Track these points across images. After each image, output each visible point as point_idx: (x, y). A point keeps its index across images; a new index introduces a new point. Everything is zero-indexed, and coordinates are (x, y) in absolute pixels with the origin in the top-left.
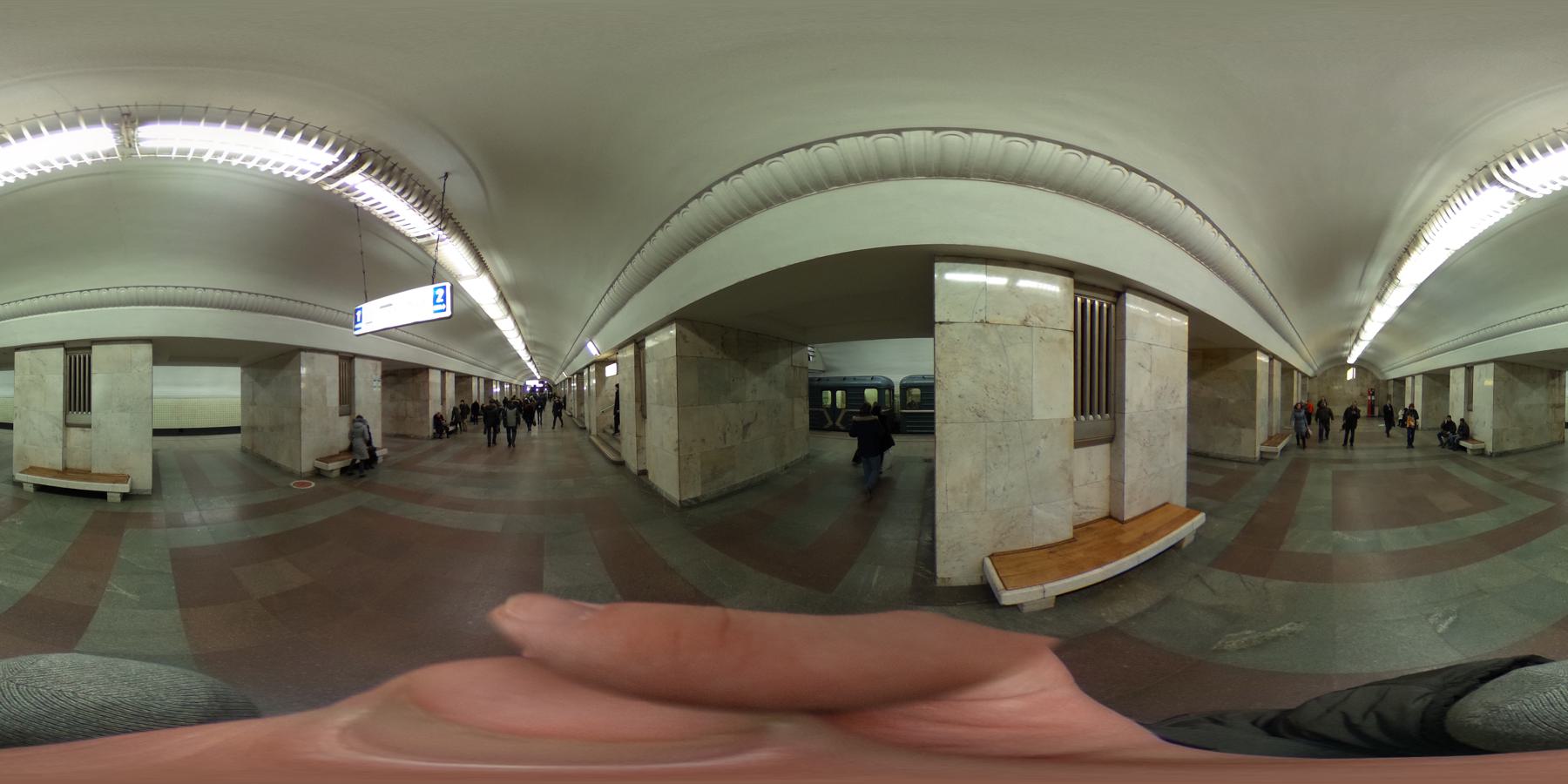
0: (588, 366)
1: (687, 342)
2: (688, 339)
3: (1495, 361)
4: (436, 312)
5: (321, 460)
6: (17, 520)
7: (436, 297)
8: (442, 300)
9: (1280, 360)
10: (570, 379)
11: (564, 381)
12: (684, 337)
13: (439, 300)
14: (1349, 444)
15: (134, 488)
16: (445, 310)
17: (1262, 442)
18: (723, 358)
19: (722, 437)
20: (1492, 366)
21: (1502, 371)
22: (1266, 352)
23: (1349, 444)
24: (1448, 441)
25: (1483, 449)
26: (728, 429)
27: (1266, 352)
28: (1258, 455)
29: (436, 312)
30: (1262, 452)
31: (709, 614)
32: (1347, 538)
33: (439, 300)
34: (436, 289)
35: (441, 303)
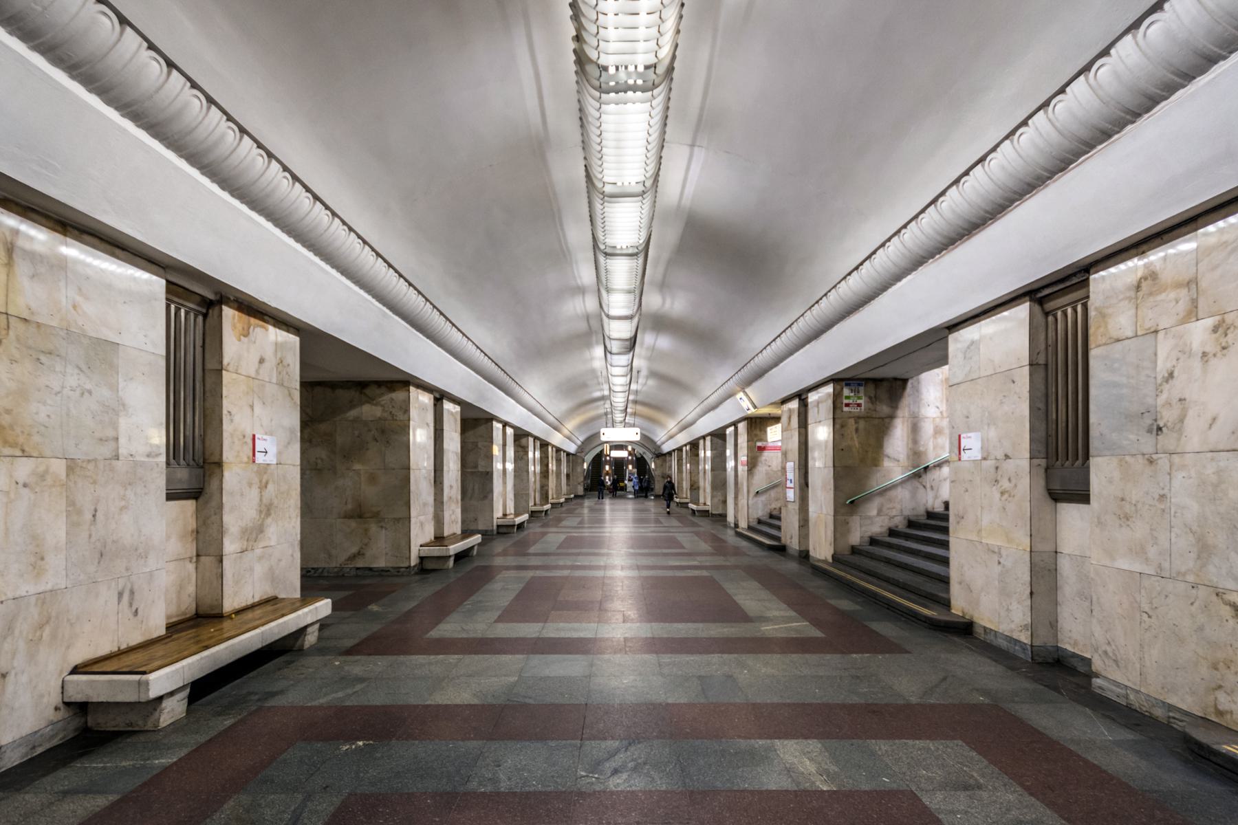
22: (500, 421)
27: (500, 421)
28: (495, 528)
30: (498, 526)
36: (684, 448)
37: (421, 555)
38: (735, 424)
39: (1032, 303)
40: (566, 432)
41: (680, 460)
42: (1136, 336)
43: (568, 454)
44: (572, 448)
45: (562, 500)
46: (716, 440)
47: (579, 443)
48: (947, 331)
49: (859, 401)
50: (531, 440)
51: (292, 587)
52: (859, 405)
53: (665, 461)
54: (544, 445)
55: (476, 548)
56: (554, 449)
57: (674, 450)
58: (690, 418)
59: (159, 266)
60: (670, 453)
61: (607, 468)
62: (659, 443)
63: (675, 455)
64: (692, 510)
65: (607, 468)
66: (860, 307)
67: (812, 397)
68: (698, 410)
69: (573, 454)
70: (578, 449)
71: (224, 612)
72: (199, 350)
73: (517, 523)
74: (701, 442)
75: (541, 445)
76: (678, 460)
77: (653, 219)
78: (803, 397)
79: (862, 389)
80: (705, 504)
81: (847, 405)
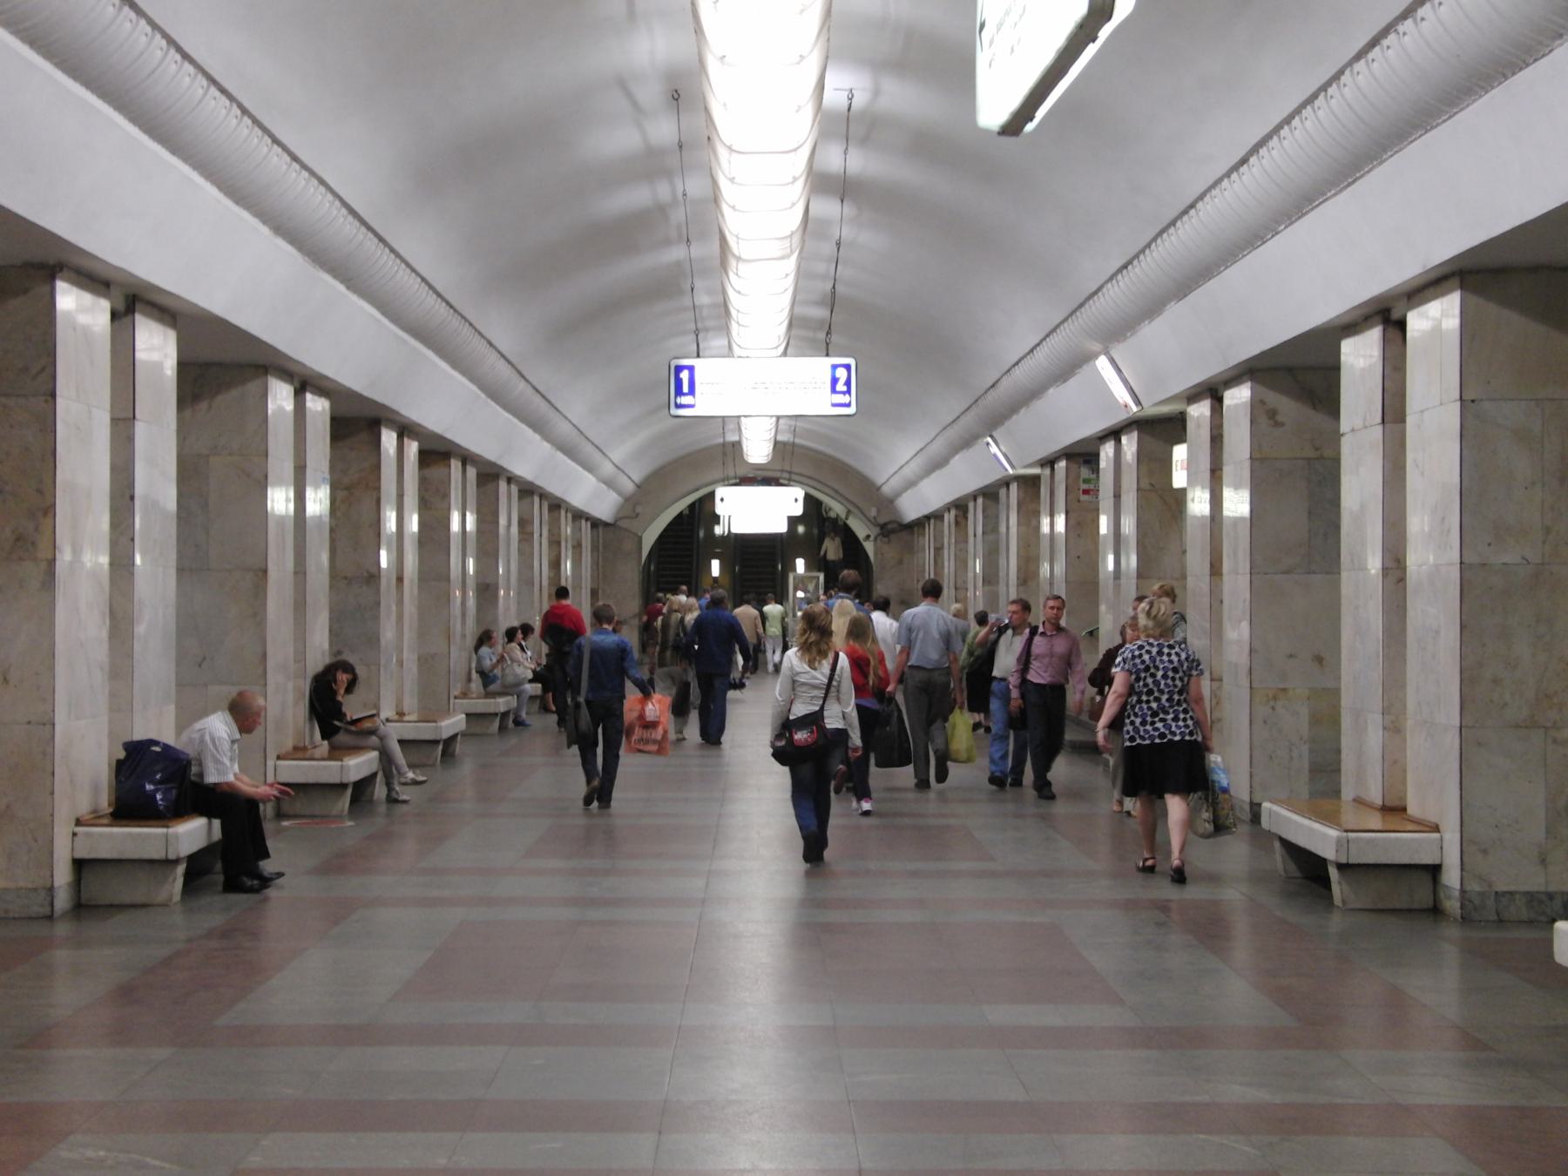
1: (1278, 424)
2: (1279, 418)
4: (834, 405)
5: (210, 733)
6: (886, 709)
7: (835, 381)
8: (845, 389)
9: (167, 311)
10: (1030, 484)
11: (990, 494)
12: (1272, 414)
13: (841, 387)
15: (105, 803)
16: (848, 405)
17: (84, 808)
22: (95, 279)
24: (1167, 679)
27: (95, 279)
28: (62, 876)
29: (834, 405)
30: (79, 865)
33: (841, 387)
34: (834, 367)
35: (844, 393)
36: (1107, 451)
38: (1213, 391)
39: (1474, 300)
40: (607, 469)
42: (1366, 427)
43: (596, 524)
44: (604, 505)
45: (453, 723)
46: (1287, 406)
47: (629, 487)
48: (1098, 441)
50: (455, 465)
51: (342, 731)
53: (910, 549)
54: (490, 475)
55: (459, 737)
56: (472, 472)
57: (974, 497)
61: (715, 567)
62: (887, 490)
63: (930, 530)
64: (1294, 851)
65: (715, 567)
66: (1415, 127)
67: (1420, 321)
68: (969, 419)
69: (606, 525)
70: (621, 508)
73: (445, 735)
74: (1003, 492)
75: (520, 491)
78: (1395, 315)
80: (1394, 810)
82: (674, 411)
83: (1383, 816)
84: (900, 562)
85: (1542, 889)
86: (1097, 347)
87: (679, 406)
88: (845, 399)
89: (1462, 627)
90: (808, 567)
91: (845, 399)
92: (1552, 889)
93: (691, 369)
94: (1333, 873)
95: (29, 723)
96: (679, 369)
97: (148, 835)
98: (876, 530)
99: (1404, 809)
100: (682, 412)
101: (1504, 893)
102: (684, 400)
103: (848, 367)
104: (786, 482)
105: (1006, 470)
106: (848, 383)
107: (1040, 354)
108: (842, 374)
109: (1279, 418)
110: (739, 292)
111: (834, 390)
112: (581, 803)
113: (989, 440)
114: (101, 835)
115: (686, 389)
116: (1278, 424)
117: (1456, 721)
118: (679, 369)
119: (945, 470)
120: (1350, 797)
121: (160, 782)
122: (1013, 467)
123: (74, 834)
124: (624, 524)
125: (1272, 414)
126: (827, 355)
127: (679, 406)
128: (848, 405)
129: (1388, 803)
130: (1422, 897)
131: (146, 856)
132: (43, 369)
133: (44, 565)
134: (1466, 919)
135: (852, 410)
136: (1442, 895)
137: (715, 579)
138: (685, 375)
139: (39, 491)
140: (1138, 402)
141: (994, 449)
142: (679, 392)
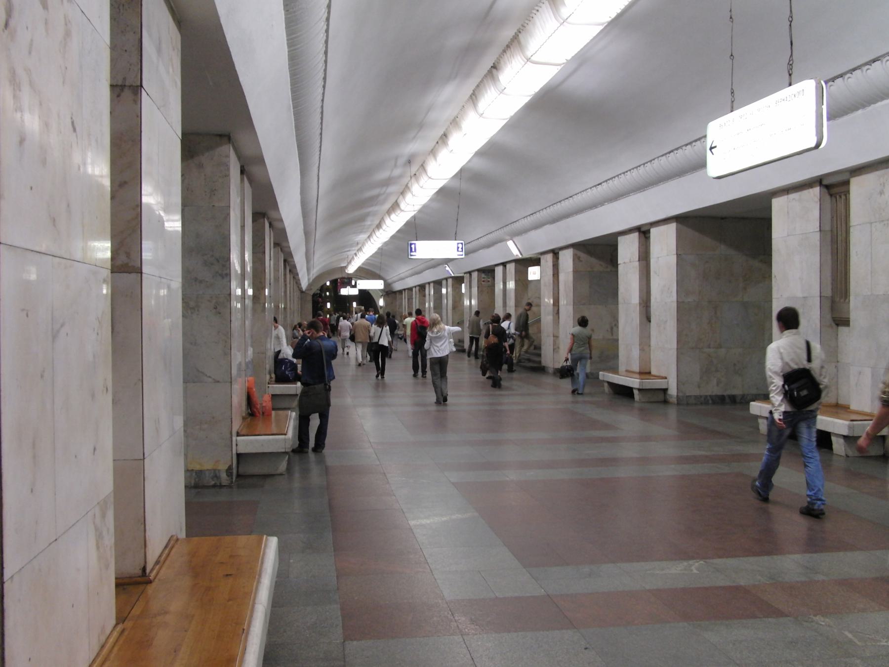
0: (415, 287)
1: (581, 261)
2: (581, 259)
3: (574, 246)
7: (458, 248)
8: (461, 250)
12: (579, 258)
13: (460, 249)
14: (420, 373)
16: (462, 255)
18: (611, 271)
19: (609, 330)
20: (672, 227)
21: (583, 256)
23: (420, 373)
25: (665, 391)
26: (226, 342)
31: (217, 537)
32: (459, 516)
33: (460, 249)
34: (458, 244)
36: (414, 289)
37: (238, 452)
39: (680, 226)
41: (410, 299)
49: (489, 280)
52: (489, 281)
57: (405, 290)
58: (402, 275)
59: (35, 251)
60: (400, 292)
63: (405, 295)
71: (819, 187)
72: (839, 226)
74: (427, 286)
76: (408, 299)
77: (846, 216)
79: (490, 274)
81: (484, 281)
82: (410, 257)
83: (639, 375)
84: (392, 303)
85: (698, 394)
86: (507, 237)
87: (411, 255)
88: (461, 253)
89: (678, 320)
90: (357, 305)
91: (461, 253)
92: (702, 394)
93: (415, 244)
94: (636, 392)
95: (258, 353)
96: (411, 244)
97: (290, 387)
98: (385, 294)
99: (650, 373)
100: (412, 257)
101: (688, 396)
102: (412, 254)
103: (462, 244)
104: (359, 277)
105: (451, 274)
106: (462, 248)
107: (314, 237)
108: (460, 246)
109: (581, 259)
110: (393, 221)
111: (458, 251)
112: (375, 377)
113: (446, 265)
114: (276, 387)
115: (413, 250)
116: (581, 261)
117: (675, 346)
118: (411, 244)
119: (419, 275)
120: (624, 370)
121: (290, 371)
122: (454, 274)
123: (268, 387)
124: (307, 292)
125: (579, 258)
126: (456, 240)
127: (411, 255)
128: (462, 255)
129: (642, 371)
130: (661, 397)
131: (290, 393)
132: (262, 245)
133: (262, 305)
134: (678, 404)
135: (463, 257)
136: (668, 397)
137: (329, 309)
138: (413, 246)
139: (261, 282)
140: (521, 254)
141: (448, 268)
142: (411, 251)
